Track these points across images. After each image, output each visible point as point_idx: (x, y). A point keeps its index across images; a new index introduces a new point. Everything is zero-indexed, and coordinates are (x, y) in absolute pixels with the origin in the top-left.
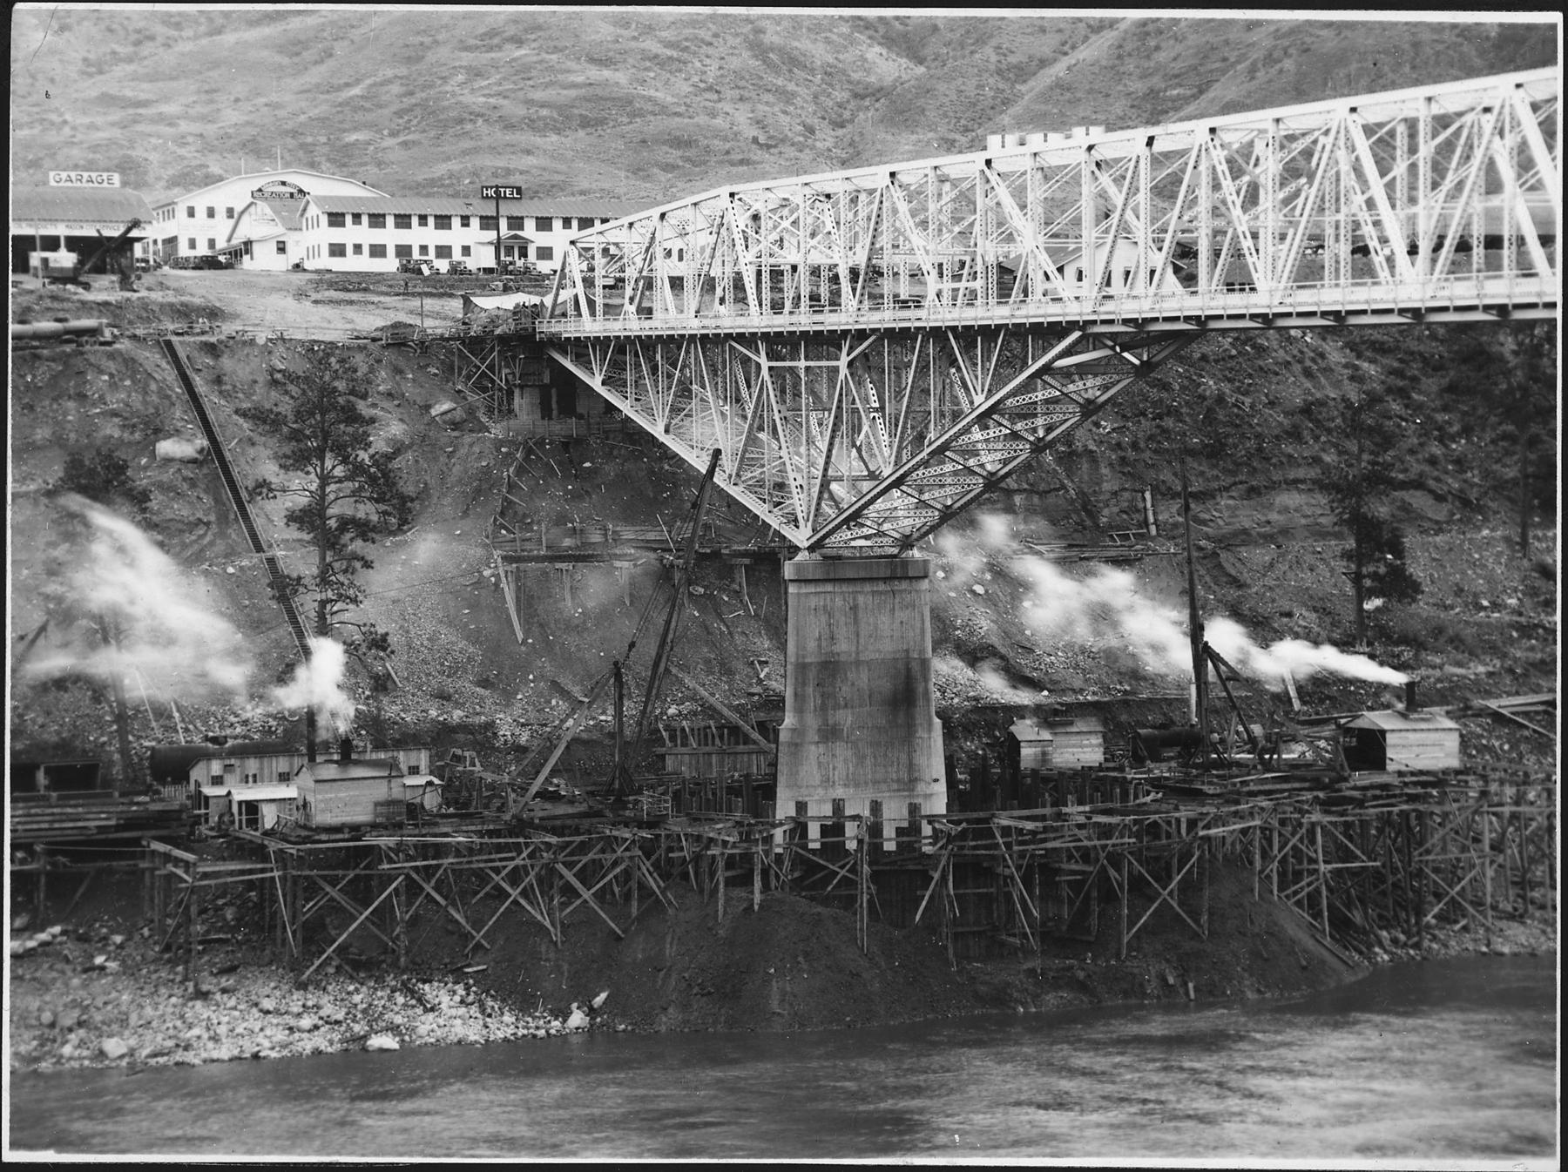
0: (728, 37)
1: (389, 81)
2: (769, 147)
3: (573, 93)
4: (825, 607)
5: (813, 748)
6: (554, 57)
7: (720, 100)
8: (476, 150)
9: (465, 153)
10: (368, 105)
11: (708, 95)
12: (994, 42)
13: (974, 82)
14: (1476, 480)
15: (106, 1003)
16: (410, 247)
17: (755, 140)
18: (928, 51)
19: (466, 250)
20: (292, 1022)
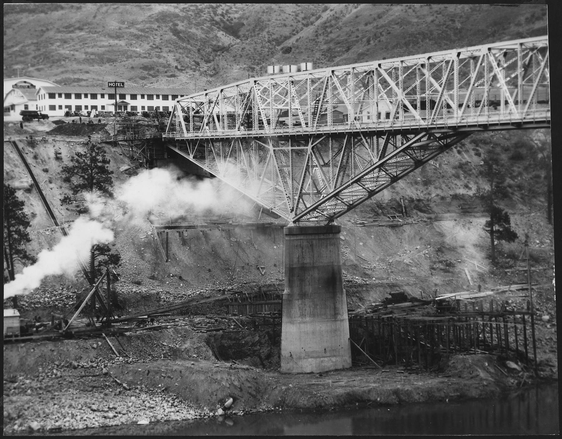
0: (164, 28)
1: (29, 45)
2: (182, 70)
3: (103, 49)
4: (300, 245)
5: (297, 302)
6: (95, 35)
7: (161, 52)
8: (66, 72)
9: (62, 72)
10: (21, 54)
11: (157, 50)
12: (267, 30)
13: (260, 45)
14: (526, 194)
15: (28, 408)
16: (81, 106)
17: (176, 67)
18: (240, 33)
19: (103, 107)
20: (106, 414)
